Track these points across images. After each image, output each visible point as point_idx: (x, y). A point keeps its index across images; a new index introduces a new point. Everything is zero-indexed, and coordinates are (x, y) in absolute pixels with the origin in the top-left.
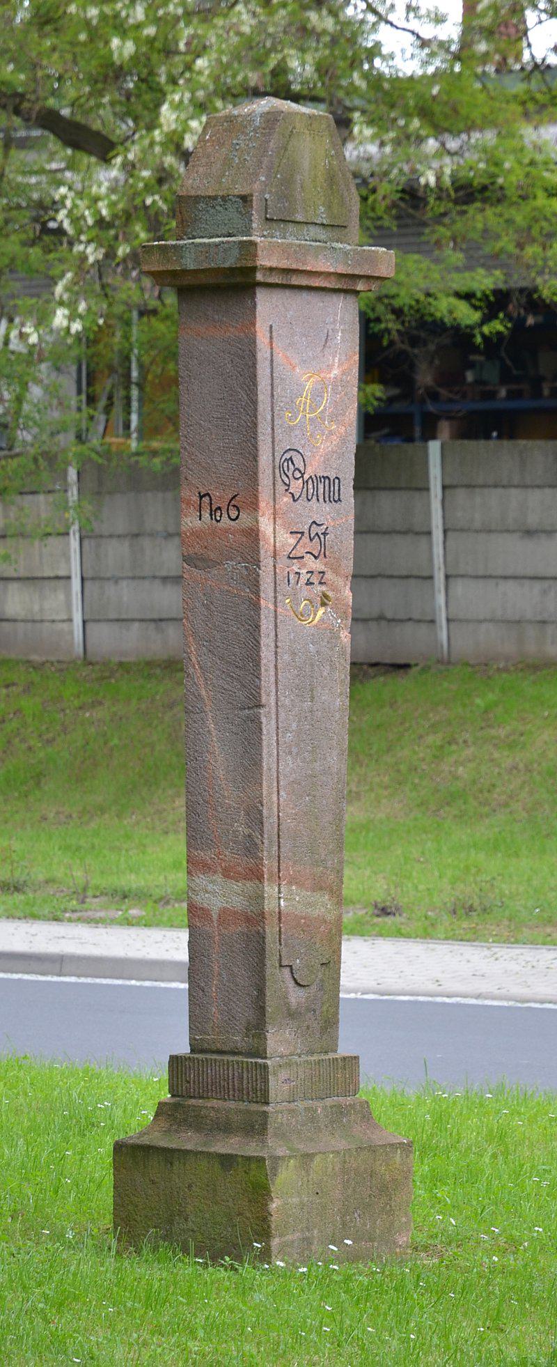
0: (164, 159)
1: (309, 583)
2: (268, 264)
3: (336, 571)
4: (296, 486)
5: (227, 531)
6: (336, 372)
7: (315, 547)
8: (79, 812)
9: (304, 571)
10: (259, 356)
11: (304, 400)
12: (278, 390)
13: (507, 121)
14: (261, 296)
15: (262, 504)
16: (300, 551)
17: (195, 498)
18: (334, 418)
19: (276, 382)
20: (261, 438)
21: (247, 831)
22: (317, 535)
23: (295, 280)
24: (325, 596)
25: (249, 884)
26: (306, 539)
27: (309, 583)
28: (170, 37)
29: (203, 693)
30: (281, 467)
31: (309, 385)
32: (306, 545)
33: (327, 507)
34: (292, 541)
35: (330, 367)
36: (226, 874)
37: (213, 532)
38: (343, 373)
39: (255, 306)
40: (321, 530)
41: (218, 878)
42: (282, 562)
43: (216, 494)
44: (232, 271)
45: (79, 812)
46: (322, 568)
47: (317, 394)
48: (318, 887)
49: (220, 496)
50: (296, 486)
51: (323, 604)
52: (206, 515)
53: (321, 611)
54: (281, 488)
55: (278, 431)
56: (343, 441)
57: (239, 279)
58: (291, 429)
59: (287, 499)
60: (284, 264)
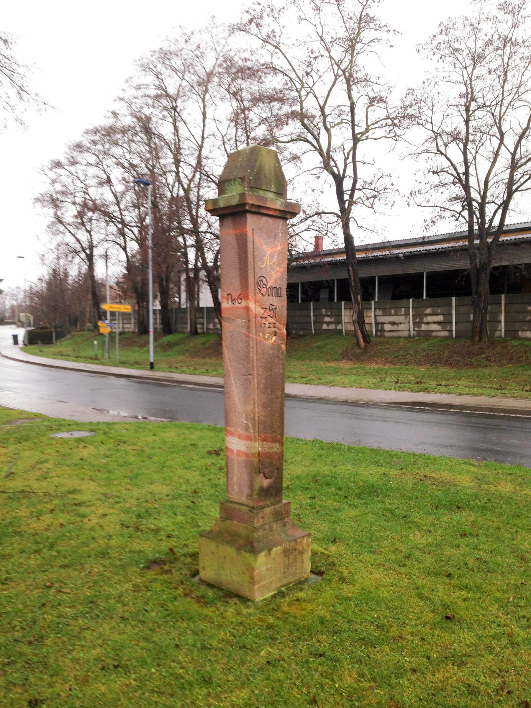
0: (216, 196)
1: (269, 327)
2: (251, 202)
3: (280, 323)
4: (264, 290)
5: (237, 308)
6: (279, 248)
7: (271, 313)
8: (148, 119)
9: (267, 323)
10: (248, 240)
11: (267, 257)
12: (256, 254)
13: (303, 667)
14: (249, 217)
15: (250, 297)
16: (265, 315)
17: (226, 296)
18: (278, 265)
19: (256, 250)
20: (249, 271)
21: (246, 422)
22: (272, 309)
23: (263, 211)
24: (276, 332)
25: (247, 442)
26: (268, 311)
27: (269, 327)
28: (250, 603)
29: (230, 369)
30: (257, 283)
31: (268, 253)
32: (268, 313)
33: (276, 299)
34: (262, 311)
35: (277, 246)
36: (239, 437)
37: (233, 308)
38: (282, 249)
39: (246, 220)
40: (273, 307)
41: (236, 438)
42: (259, 319)
43: (233, 294)
44: (237, 206)
45: (148, 119)
46: (274, 321)
47: (272, 256)
48: (274, 441)
49: (235, 294)
50: (264, 290)
51: (275, 335)
52: (230, 302)
53: (274, 338)
54: (258, 291)
55: (256, 269)
56: (283, 274)
57: (240, 209)
58: (261, 268)
59: (260, 295)
60: (257, 203)
